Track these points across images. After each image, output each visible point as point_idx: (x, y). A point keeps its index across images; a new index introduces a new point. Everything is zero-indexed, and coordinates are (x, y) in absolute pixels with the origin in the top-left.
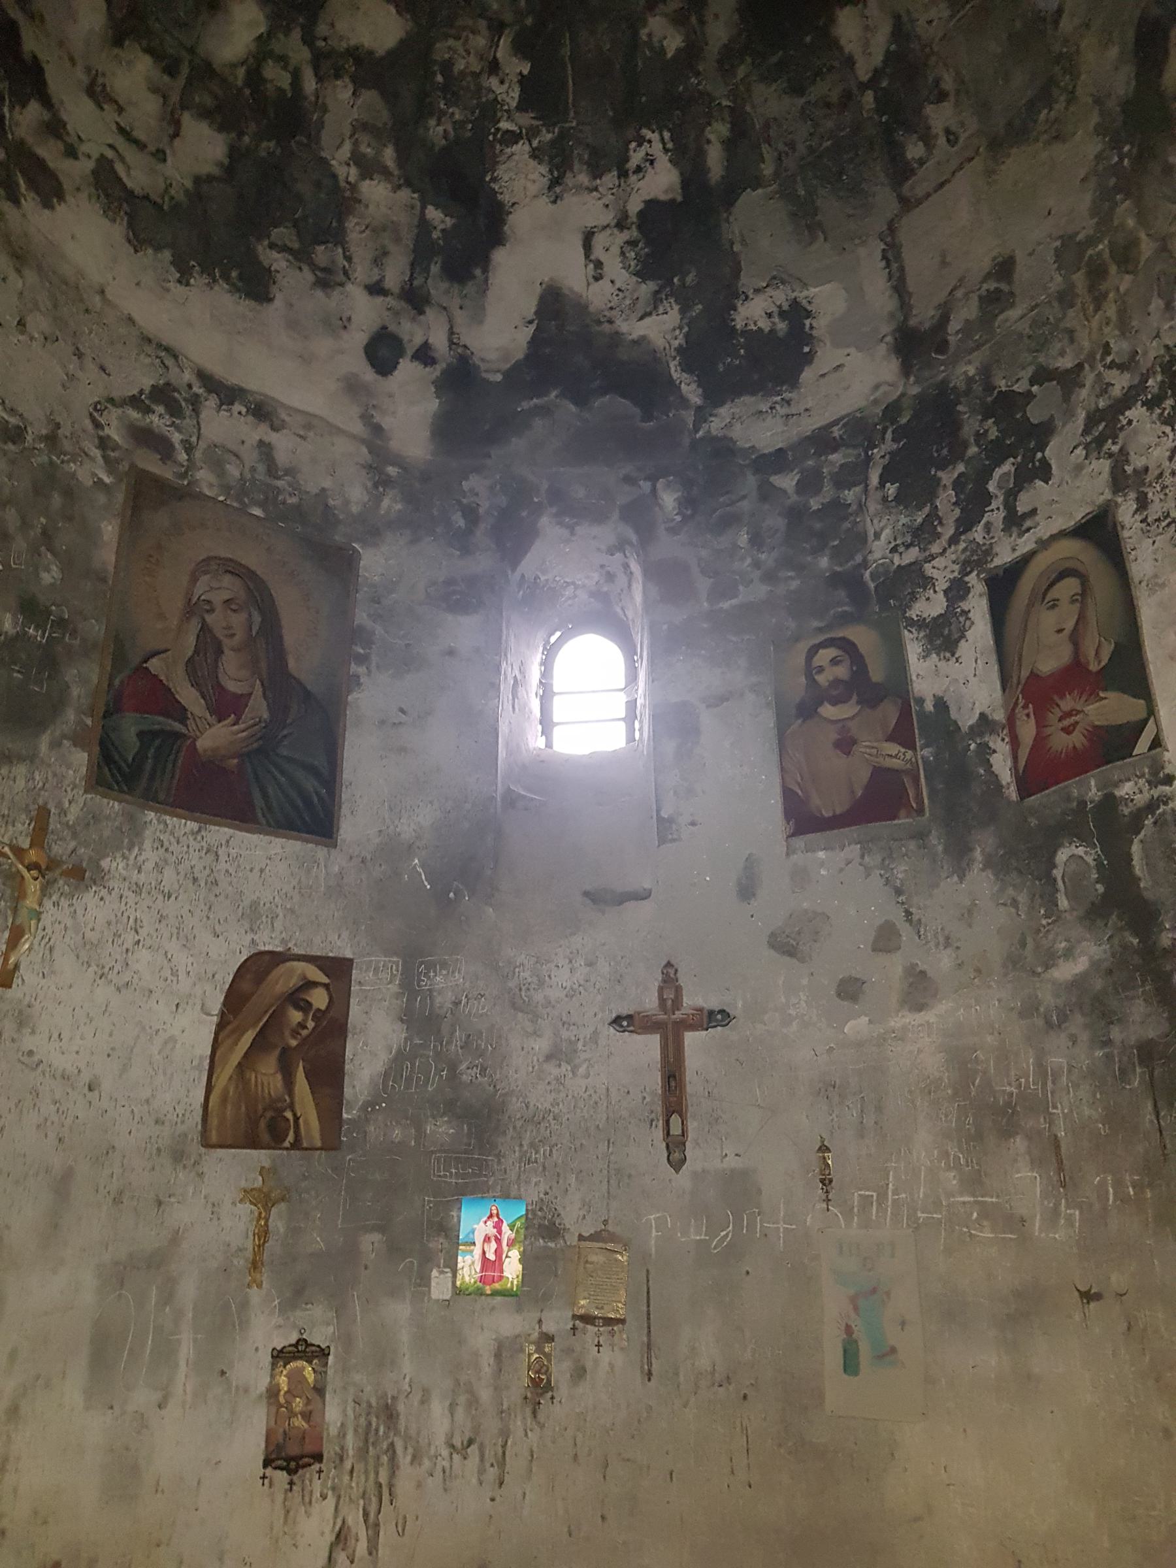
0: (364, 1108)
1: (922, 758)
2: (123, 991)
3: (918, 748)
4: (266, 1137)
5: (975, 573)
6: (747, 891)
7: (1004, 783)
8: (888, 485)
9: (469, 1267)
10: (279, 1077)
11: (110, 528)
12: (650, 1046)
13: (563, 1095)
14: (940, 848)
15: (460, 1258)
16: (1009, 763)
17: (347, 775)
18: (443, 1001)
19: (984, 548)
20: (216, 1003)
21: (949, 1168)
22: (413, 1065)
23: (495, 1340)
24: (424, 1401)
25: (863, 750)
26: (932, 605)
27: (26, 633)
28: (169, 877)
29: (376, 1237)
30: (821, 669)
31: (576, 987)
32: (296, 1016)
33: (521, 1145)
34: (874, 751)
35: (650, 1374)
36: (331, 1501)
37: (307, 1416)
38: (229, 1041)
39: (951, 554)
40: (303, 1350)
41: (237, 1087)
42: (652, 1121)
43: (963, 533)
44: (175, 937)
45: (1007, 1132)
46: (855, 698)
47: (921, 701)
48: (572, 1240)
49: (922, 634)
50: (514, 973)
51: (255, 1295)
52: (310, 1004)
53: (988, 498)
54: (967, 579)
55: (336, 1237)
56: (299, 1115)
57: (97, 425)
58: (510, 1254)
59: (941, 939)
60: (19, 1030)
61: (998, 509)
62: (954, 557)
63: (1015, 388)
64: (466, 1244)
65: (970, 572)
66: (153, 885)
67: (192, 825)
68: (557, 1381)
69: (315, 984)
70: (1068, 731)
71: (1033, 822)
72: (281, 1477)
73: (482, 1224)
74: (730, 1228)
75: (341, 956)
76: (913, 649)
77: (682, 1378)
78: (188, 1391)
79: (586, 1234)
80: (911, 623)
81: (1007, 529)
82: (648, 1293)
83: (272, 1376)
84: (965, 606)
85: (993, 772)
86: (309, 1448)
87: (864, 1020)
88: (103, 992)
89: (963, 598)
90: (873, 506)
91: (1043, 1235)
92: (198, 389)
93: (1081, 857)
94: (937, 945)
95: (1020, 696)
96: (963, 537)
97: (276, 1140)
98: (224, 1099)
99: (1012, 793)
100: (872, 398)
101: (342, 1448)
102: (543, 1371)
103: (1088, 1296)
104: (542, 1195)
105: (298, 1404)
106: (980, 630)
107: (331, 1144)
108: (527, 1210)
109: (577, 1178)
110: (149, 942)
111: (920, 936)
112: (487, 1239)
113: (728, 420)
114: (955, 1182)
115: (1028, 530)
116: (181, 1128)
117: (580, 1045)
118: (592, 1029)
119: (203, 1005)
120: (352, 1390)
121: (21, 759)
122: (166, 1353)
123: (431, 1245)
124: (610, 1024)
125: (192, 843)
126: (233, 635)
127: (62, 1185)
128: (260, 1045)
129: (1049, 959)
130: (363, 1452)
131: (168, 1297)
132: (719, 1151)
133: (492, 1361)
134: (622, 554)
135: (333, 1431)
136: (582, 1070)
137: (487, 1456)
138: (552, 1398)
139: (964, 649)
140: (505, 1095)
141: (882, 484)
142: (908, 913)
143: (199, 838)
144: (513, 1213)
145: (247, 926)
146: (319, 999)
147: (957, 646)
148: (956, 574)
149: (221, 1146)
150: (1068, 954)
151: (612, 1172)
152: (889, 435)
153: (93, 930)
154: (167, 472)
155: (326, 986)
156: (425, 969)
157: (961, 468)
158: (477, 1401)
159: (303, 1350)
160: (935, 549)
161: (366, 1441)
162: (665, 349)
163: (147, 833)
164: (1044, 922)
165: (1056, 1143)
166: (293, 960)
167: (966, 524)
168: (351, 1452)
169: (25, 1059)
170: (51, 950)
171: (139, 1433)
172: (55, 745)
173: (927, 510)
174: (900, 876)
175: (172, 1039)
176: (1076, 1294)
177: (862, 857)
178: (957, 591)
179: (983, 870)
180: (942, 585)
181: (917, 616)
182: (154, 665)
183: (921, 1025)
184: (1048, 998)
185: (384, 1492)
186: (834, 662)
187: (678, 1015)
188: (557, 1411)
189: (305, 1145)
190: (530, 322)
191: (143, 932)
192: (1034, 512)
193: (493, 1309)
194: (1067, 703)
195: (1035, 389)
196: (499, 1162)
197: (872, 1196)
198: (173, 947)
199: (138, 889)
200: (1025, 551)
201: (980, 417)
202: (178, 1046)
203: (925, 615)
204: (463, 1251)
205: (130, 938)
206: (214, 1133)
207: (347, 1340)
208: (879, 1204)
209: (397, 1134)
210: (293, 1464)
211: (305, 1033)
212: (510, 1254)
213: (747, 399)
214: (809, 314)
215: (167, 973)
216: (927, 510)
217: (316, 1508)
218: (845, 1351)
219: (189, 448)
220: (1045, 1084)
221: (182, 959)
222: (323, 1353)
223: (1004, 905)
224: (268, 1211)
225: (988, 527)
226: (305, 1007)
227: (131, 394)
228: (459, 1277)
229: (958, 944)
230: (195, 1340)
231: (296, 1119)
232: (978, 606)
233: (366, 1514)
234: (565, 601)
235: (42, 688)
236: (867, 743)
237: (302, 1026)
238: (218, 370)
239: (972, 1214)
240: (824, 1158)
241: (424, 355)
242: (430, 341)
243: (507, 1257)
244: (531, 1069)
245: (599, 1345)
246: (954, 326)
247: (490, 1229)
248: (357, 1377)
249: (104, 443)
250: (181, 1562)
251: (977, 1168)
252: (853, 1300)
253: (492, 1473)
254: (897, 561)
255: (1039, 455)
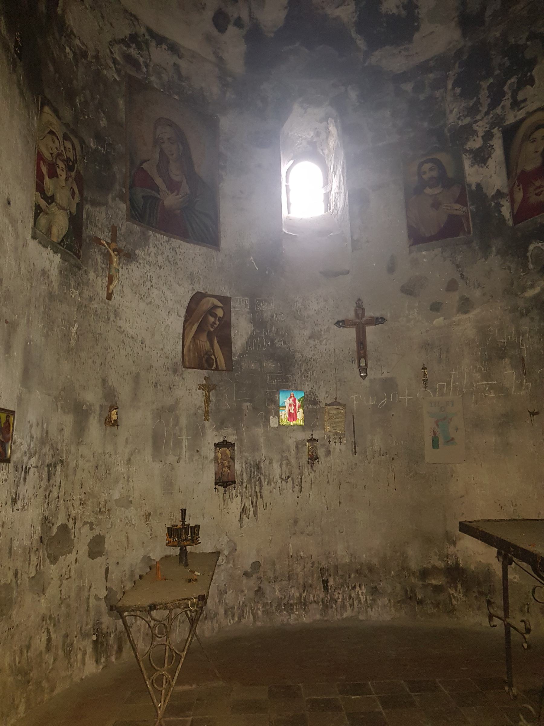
0: (239, 356)
1: (471, 210)
2: (149, 305)
3: (468, 205)
4: (206, 365)
5: (497, 128)
6: (391, 269)
7: (507, 219)
8: (456, 88)
9: (284, 414)
10: (208, 343)
11: (121, 102)
12: (351, 333)
13: (316, 352)
14: (477, 248)
15: (280, 412)
16: (509, 211)
17: (222, 219)
18: (267, 315)
19: (501, 117)
20: (183, 312)
21: (476, 372)
22: (257, 340)
23: (296, 441)
24: (271, 463)
25: (444, 207)
26: (476, 143)
27: (98, 148)
28: (160, 260)
29: (249, 404)
30: (425, 173)
31: (320, 310)
32: (212, 319)
33: (301, 371)
34: (449, 208)
35: (355, 452)
36: (239, 498)
37: (229, 468)
38: (189, 328)
39: (486, 120)
40: (225, 444)
41: (193, 346)
42: (353, 361)
43: (491, 110)
44: (165, 284)
45: (501, 358)
46: (440, 186)
47: (470, 185)
48: (323, 405)
49: (471, 156)
50: (294, 305)
51: (207, 424)
52: (216, 315)
53: (504, 94)
54: (492, 131)
55: (234, 404)
56: (217, 357)
57: (111, 52)
58: (299, 410)
59: (476, 284)
60: (115, 318)
61: (508, 99)
62: (487, 121)
63: (519, 43)
64: (282, 407)
65: (494, 128)
66: (155, 263)
67: (166, 238)
68: (320, 456)
69: (218, 307)
70: (537, 194)
71: (520, 234)
72: (221, 489)
73: (288, 400)
74: (386, 399)
75: (226, 296)
76: (467, 163)
77: (368, 453)
78: (187, 457)
79: (328, 403)
80: (466, 151)
81: (512, 108)
82: (354, 424)
83: (215, 453)
84: (492, 143)
85: (502, 215)
86: (230, 478)
87: (442, 318)
88: (142, 305)
89: (491, 139)
90: (449, 98)
91: (515, 393)
92: (147, 37)
93: (539, 247)
94: (474, 287)
95: (516, 181)
96: (492, 112)
97: (209, 366)
98: (189, 350)
99: (510, 223)
100: (448, 48)
101: (242, 479)
102: (314, 452)
103: (533, 414)
104: (310, 389)
105: (226, 463)
106: (498, 153)
107: (229, 369)
108: (305, 395)
109: (323, 383)
110: (156, 286)
111: (467, 284)
112: (290, 405)
113: (379, 58)
114: (479, 377)
115: (523, 107)
116: (175, 361)
117: (322, 333)
118: (327, 327)
119: (178, 313)
120: (244, 458)
121: (103, 205)
122: (178, 443)
123: (269, 407)
124: (335, 324)
125: (167, 246)
126: (173, 155)
127: (137, 379)
128: (200, 330)
129: (524, 289)
130: (249, 481)
131: (177, 423)
132: (380, 371)
133: (295, 449)
134: (326, 123)
135: (238, 473)
136: (324, 342)
137: (295, 482)
138: (318, 461)
139: (491, 162)
140: (294, 352)
141: (453, 88)
142: (462, 275)
143: (169, 244)
144: (299, 395)
145: (190, 282)
146: (220, 313)
147: (487, 161)
148: (487, 129)
149: (190, 368)
150: (532, 286)
151: (338, 381)
152: (457, 65)
153: (136, 279)
154: (140, 76)
155: (222, 308)
156: (259, 302)
157: (491, 80)
158: (290, 463)
159: (225, 444)
160: (478, 117)
161: (250, 477)
162: (348, 23)
163: (150, 240)
164: (522, 274)
165: (523, 359)
166: (208, 297)
167: (492, 106)
168: (245, 481)
169: (118, 329)
170: (122, 286)
171: (171, 471)
172: (114, 199)
173: (475, 99)
174: (459, 260)
175: (168, 326)
176: (528, 413)
177: (442, 253)
178: (488, 136)
179: (496, 255)
180: (481, 134)
181: (469, 148)
182: (145, 166)
183: (466, 319)
184: (521, 304)
185: (258, 495)
186: (431, 169)
187: (364, 319)
188: (322, 465)
189: (220, 369)
190: (286, 8)
191: (154, 281)
192: (525, 100)
193: (294, 430)
194: (538, 183)
195: (529, 43)
196: (293, 377)
197: (444, 384)
198: (164, 288)
199: (149, 263)
200: (521, 117)
201: (501, 57)
202: (170, 329)
203: (473, 148)
204: (281, 409)
205: (149, 284)
206: (187, 363)
207: (241, 441)
208: (447, 388)
209: (253, 366)
210: (225, 484)
211: (216, 326)
212: (299, 410)
213: (388, 47)
214: (417, 7)
215: (163, 299)
216: (475, 99)
217: (234, 500)
218: (433, 441)
219: (147, 66)
220: (519, 337)
221: (168, 294)
222: (233, 445)
223: (505, 269)
224: (209, 392)
225: (503, 107)
226: (215, 316)
227: (122, 38)
228: (280, 419)
229: (484, 286)
230: (187, 439)
231: (216, 359)
232: (497, 143)
233: (252, 502)
234: (297, 145)
235: (106, 174)
236: (446, 205)
237: (214, 323)
238: (154, 27)
239: (486, 388)
240: (424, 371)
241: (239, 23)
242: (241, 16)
243: (298, 411)
244: (303, 342)
245: (335, 443)
246: (488, 13)
247: (291, 401)
248: (246, 454)
249: (115, 61)
250: (190, 516)
251: (488, 371)
252: (437, 423)
253: (297, 488)
254: (460, 123)
255: (529, 74)
